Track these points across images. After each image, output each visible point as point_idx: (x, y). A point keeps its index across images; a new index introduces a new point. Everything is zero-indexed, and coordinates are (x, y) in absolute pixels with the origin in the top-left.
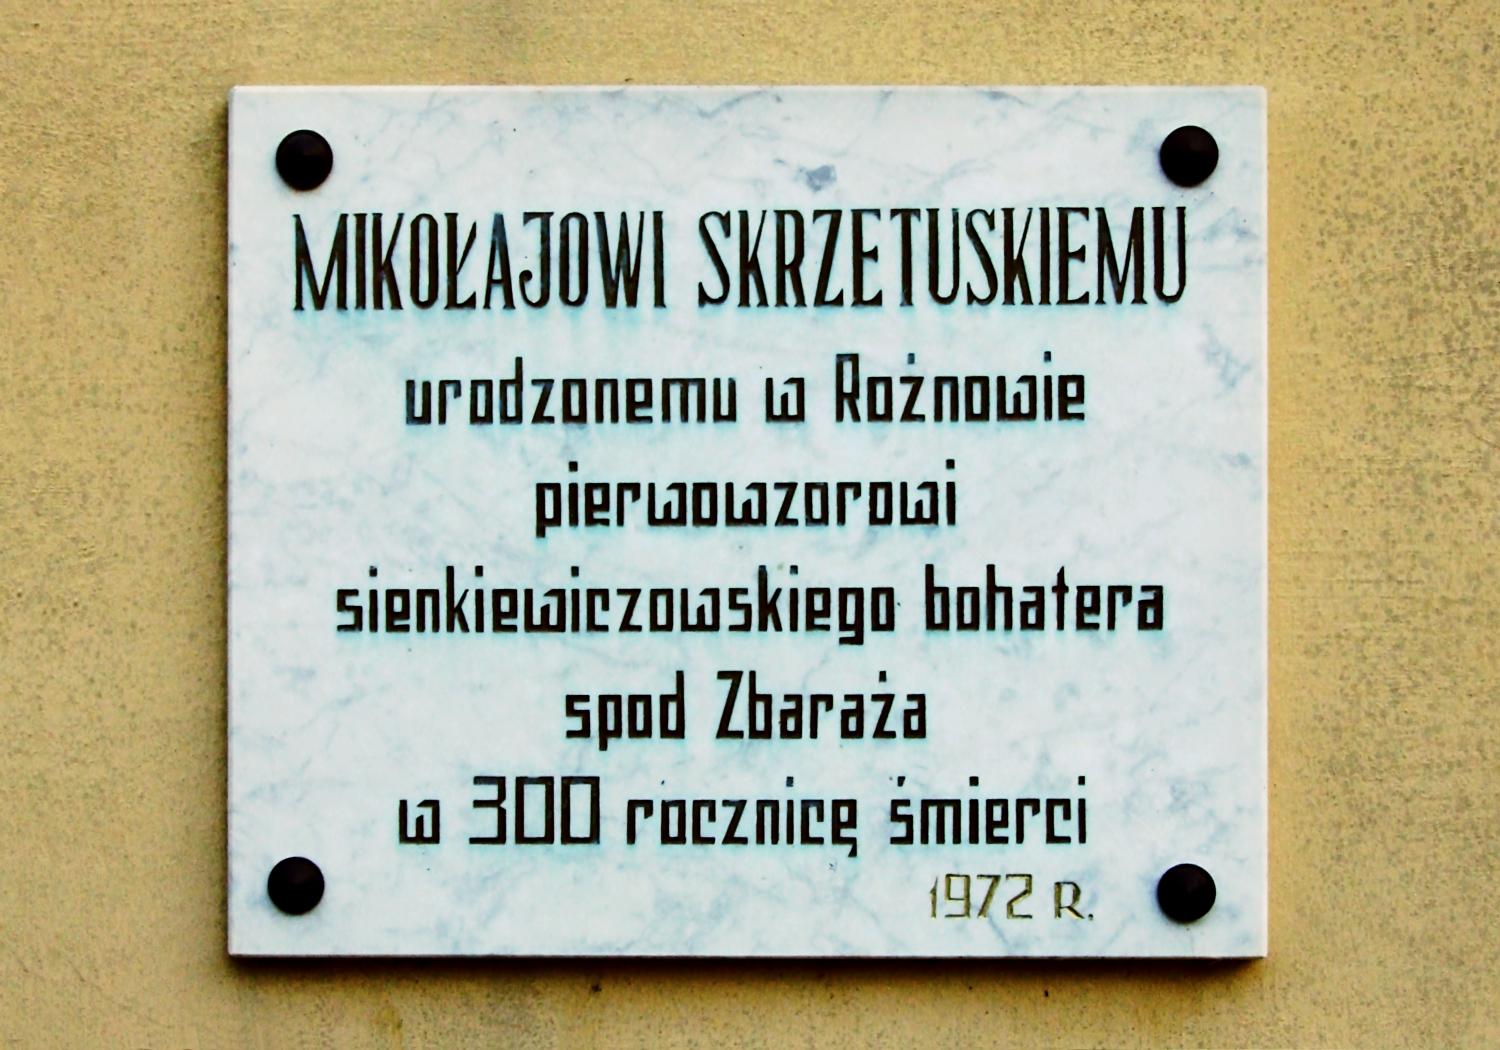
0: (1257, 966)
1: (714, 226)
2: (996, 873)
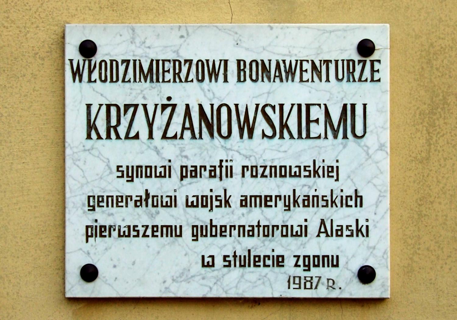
0: (387, 300)
1: (269, 110)
2: (320, 276)
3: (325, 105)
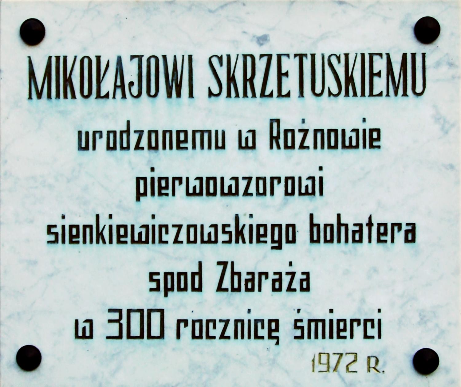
1: (334, 60)
3: (388, 55)
